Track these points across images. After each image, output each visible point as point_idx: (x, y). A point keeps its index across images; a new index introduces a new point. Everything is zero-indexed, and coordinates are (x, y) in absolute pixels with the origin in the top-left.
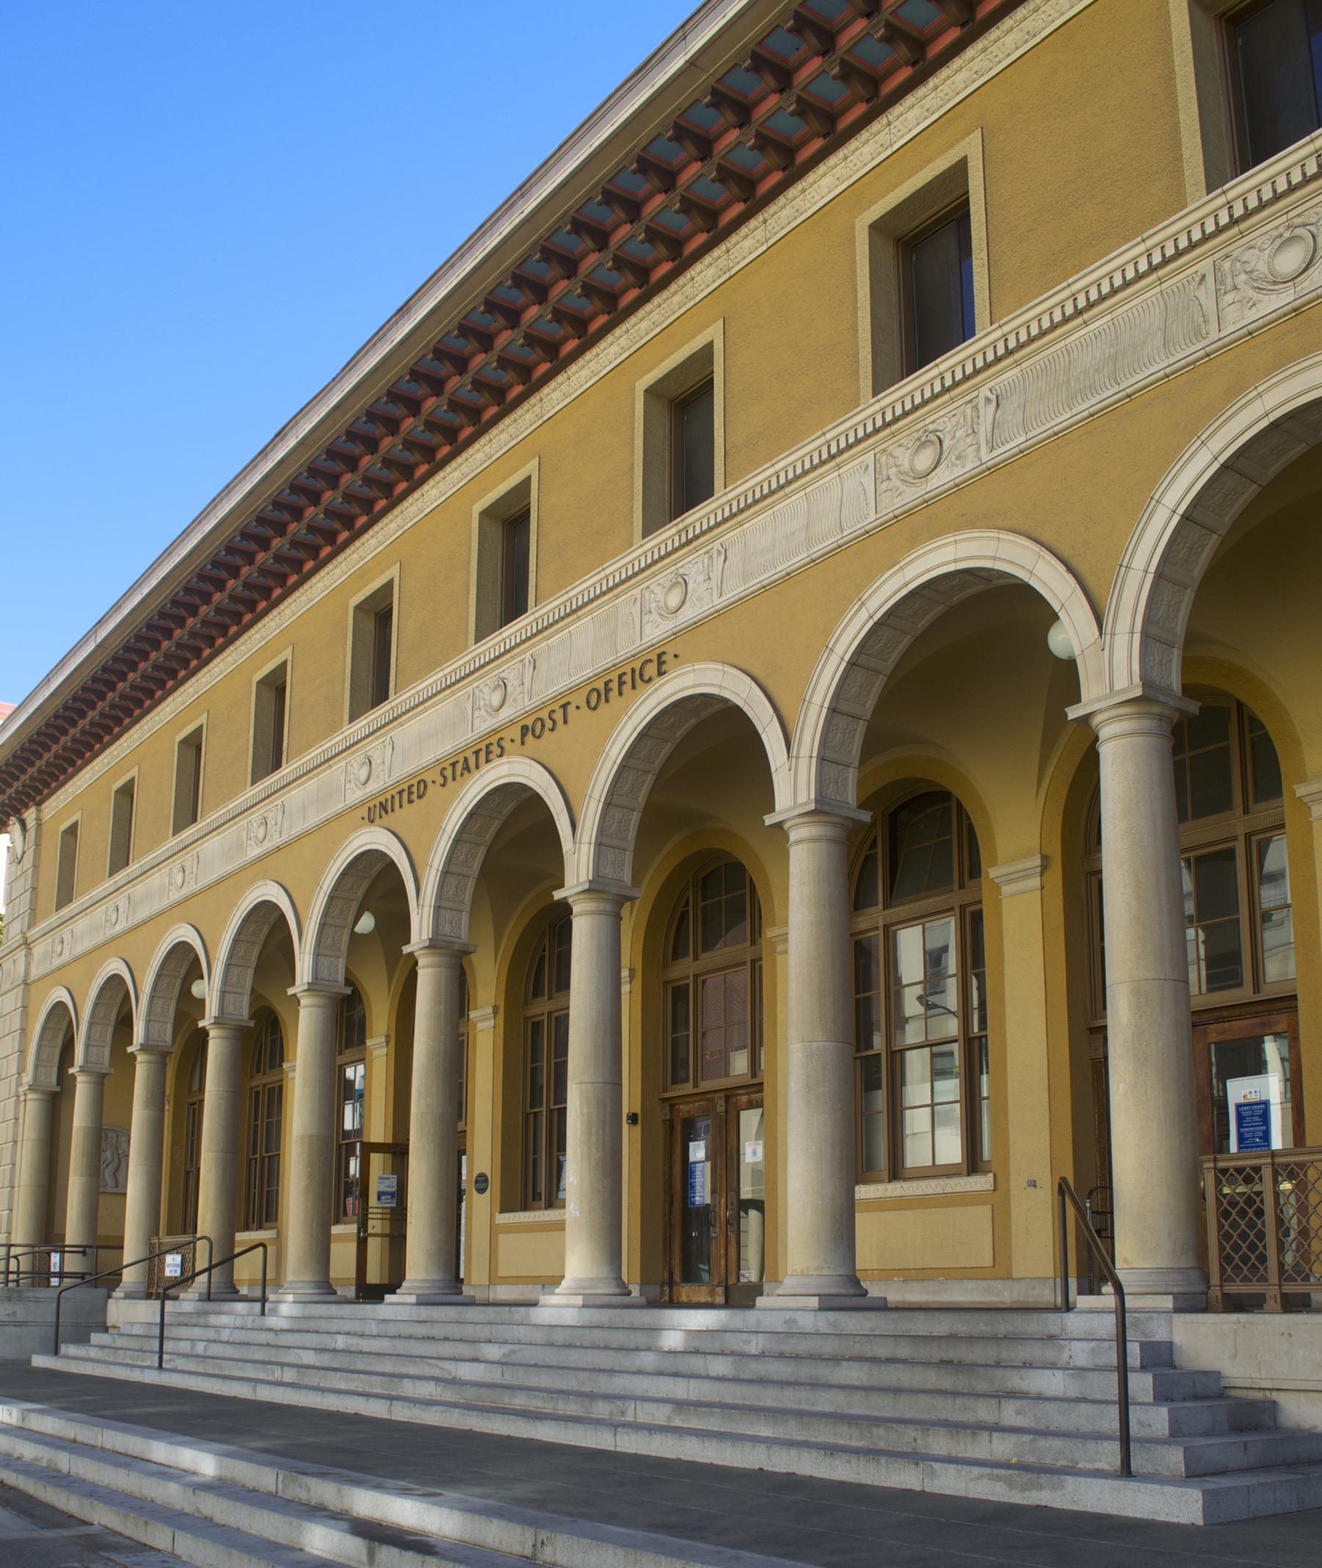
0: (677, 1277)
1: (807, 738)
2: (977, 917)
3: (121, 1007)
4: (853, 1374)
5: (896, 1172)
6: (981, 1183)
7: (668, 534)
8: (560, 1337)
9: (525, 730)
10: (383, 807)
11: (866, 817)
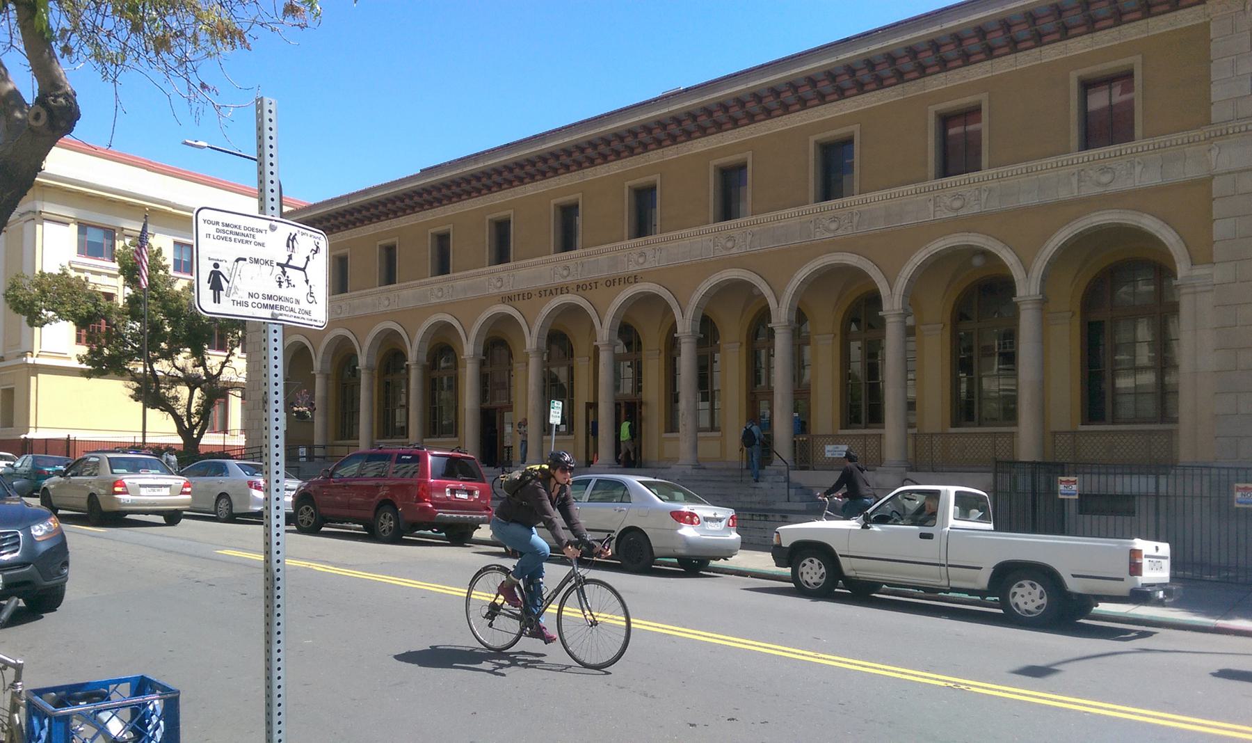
9: (578, 286)
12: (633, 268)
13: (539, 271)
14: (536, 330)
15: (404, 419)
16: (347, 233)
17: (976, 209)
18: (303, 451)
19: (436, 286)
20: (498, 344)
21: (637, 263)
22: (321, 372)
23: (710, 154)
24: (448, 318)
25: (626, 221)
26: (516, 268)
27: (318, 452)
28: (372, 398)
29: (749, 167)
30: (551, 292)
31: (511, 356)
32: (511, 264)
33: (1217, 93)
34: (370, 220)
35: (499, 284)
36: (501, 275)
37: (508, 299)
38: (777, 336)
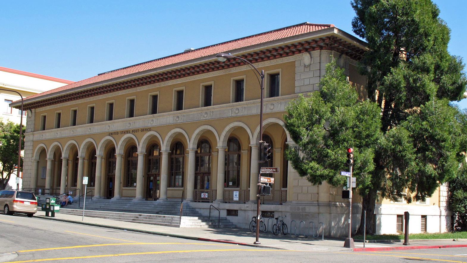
0: (148, 197)
1: (255, 136)
2: (240, 155)
3: (283, 135)
4: (165, 207)
5: (175, 186)
6: (182, 188)
7: (152, 115)
8: (136, 203)
9: (133, 131)
10: (112, 134)
11: (170, 152)
12: (149, 125)
13: (66, 132)
14: (192, 140)
15: (235, 173)
16: (44, 108)
17: (242, 114)
18: (40, 191)
19: (88, 128)
20: (205, 143)
21: (236, 113)
22: (81, 157)
23: (174, 86)
24: (92, 140)
25: (126, 111)
26: (160, 116)
27: (47, 191)
28: (121, 168)
29: (184, 92)
30: (124, 133)
31: (210, 148)
32: (183, 111)
33: (297, 84)
34: (124, 88)
35: (237, 112)
36: (238, 107)
37: (111, 134)
38: (48, 162)
